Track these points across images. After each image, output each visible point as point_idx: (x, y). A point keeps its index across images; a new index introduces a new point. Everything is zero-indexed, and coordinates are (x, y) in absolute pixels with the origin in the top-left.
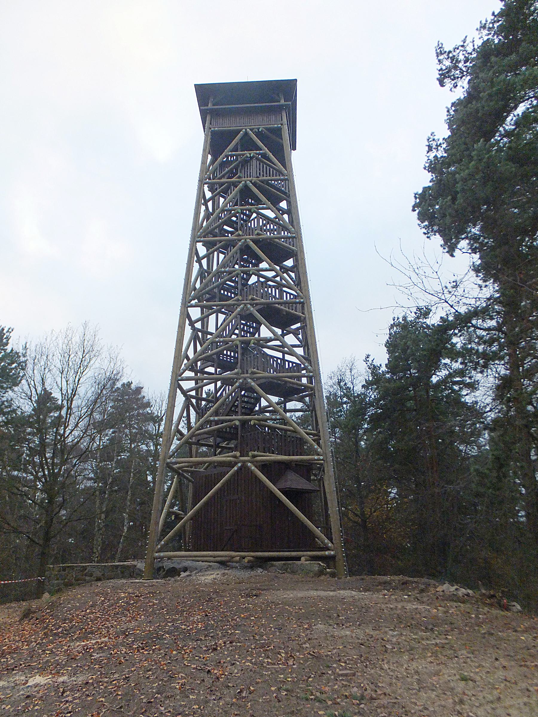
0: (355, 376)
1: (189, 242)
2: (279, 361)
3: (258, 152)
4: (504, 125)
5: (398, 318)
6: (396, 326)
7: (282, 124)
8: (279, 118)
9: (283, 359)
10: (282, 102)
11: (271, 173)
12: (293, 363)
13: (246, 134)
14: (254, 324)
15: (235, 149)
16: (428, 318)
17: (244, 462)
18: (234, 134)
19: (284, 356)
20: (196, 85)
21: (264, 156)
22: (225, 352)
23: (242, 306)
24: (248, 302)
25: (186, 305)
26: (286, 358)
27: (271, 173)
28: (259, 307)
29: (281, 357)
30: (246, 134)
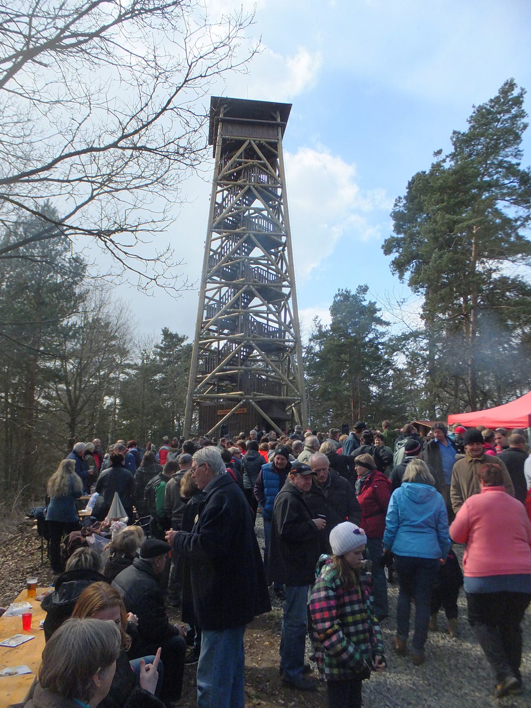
0: (55, 121)
1: (206, 231)
3: (259, 161)
5: (342, 290)
6: (340, 296)
7: (278, 140)
8: (276, 132)
10: (279, 120)
12: (275, 328)
13: (250, 143)
15: (240, 157)
16: (366, 294)
17: (247, 399)
18: (240, 143)
19: (268, 323)
20: (212, 97)
21: (264, 165)
23: (246, 286)
24: (251, 283)
26: (269, 324)
28: (257, 287)
30: (250, 143)
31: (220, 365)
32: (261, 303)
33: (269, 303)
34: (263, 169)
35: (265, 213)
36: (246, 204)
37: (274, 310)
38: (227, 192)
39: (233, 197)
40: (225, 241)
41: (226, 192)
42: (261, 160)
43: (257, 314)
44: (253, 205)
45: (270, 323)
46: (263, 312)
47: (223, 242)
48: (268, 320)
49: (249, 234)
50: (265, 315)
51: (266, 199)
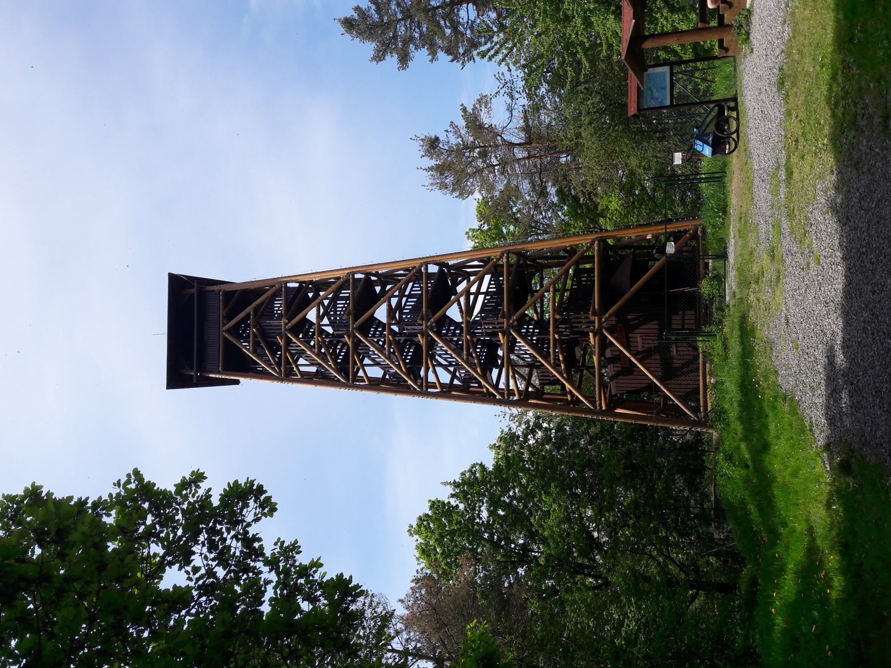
2: (488, 297)
4: (517, 344)
9: (486, 294)
11: (269, 314)
12: (490, 284)
13: (228, 331)
14: (451, 328)
19: (482, 293)
22: (478, 350)
25: (424, 389)
27: (269, 314)
28: (430, 313)
29: (484, 295)
30: (228, 331)
31: (322, 363)
32: (456, 305)
33: (455, 293)
34: (267, 310)
35: (394, 301)
36: (384, 330)
37: (465, 283)
38: (366, 359)
39: (519, 347)
40: (437, 361)
41: (367, 361)
42: (250, 313)
43: (470, 309)
44: (314, 320)
45: (484, 289)
46: (468, 299)
47: (440, 365)
48: (478, 292)
49: (286, 330)
50: (472, 297)
51: (306, 303)
